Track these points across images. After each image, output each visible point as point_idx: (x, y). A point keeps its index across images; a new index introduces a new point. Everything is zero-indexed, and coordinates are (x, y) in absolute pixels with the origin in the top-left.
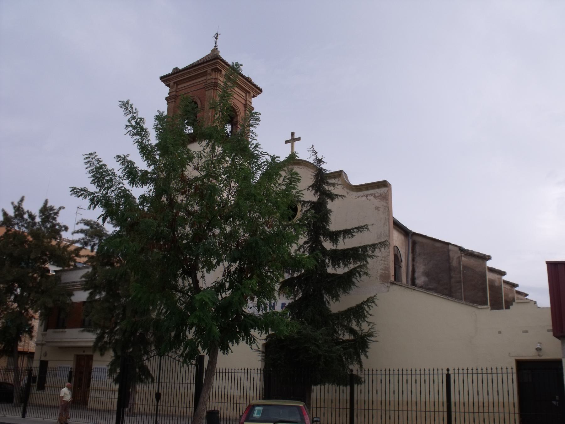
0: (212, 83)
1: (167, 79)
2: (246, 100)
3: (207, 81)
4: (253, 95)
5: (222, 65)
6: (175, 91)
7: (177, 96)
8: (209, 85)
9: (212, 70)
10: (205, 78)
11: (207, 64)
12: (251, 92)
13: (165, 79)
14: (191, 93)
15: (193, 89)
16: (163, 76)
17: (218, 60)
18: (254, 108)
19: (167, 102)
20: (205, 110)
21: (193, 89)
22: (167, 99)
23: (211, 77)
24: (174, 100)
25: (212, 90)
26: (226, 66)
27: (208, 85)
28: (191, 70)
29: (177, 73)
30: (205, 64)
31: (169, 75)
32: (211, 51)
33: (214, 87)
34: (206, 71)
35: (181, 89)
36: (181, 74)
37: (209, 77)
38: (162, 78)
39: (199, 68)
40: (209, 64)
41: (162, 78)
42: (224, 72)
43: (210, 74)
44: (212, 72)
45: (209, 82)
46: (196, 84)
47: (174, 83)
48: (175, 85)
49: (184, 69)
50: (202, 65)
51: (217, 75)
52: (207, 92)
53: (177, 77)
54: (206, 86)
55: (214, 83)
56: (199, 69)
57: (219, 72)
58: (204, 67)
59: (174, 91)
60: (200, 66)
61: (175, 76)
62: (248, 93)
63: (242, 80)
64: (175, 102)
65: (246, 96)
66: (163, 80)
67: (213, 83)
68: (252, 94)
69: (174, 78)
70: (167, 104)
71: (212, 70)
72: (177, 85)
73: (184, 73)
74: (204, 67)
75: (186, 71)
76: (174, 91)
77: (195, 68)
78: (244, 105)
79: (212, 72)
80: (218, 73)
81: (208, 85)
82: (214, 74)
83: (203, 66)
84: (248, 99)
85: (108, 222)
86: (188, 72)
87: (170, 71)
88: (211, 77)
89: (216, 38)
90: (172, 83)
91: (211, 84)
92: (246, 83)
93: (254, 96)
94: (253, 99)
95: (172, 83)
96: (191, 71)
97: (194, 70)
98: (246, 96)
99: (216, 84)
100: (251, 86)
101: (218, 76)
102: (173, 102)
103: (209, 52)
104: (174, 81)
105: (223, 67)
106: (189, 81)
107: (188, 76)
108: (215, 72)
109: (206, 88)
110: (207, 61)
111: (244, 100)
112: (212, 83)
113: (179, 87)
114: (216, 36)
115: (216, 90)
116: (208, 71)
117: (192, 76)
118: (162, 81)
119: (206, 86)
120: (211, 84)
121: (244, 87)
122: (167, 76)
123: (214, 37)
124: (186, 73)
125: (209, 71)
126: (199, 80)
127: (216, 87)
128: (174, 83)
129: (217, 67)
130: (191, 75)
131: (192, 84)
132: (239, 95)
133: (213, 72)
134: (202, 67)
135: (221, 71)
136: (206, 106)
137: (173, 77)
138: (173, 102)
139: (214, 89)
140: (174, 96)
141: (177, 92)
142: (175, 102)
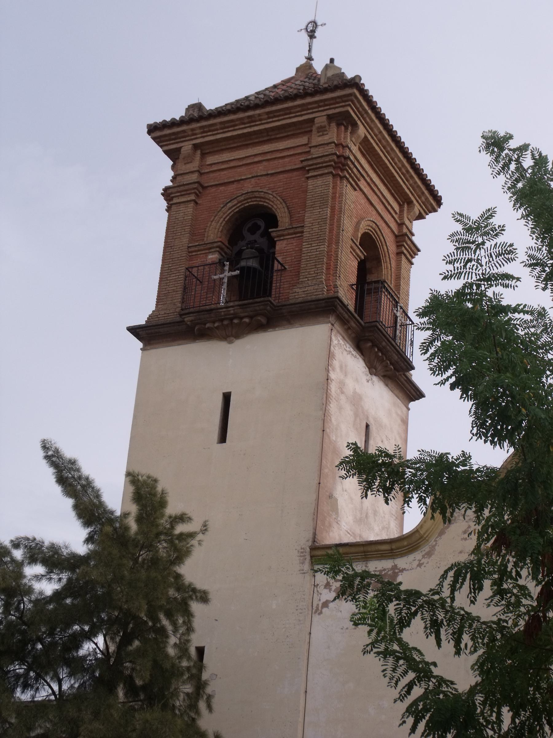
0: (331, 158)
1: (174, 134)
2: (401, 225)
3: (313, 150)
4: (417, 213)
5: (361, 105)
6: (198, 171)
7: (204, 188)
8: (319, 160)
9: (330, 118)
10: (303, 140)
11: (316, 98)
12: (415, 202)
13: (167, 132)
14: (253, 180)
15: (260, 169)
16: (168, 119)
17: (355, 91)
18: (419, 250)
19: (165, 204)
20: (306, 234)
21: (260, 169)
22: (167, 193)
23: (326, 139)
24: (193, 197)
25: (330, 178)
26: (370, 112)
27: (315, 161)
28: (258, 112)
29: (201, 118)
30: (309, 100)
31: (173, 123)
32: (298, 70)
33: (334, 168)
34: (312, 120)
35: (215, 168)
36: (221, 123)
37: (316, 140)
38: (153, 129)
39: (287, 108)
40: (321, 101)
41: (153, 129)
42: (362, 131)
43: (322, 130)
44: (329, 123)
45: (316, 152)
46: (268, 157)
47: (196, 147)
48: (199, 152)
49: (220, 112)
50: (299, 102)
51: (343, 136)
52: (310, 182)
53: (205, 130)
54: (310, 162)
55: (338, 157)
56: (288, 111)
57: (350, 128)
58: (304, 107)
59: (192, 172)
60: (290, 104)
61: (201, 127)
62: (406, 206)
63: (400, 160)
64: (196, 203)
65: (401, 211)
66: (158, 134)
67: (335, 157)
68: (417, 209)
69: (198, 131)
70: (168, 210)
71: (330, 118)
72: (203, 155)
73: (232, 121)
74: (304, 107)
75: (241, 115)
76: (192, 172)
77: (274, 108)
78: (396, 236)
79: (329, 123)
80: (346, 128)
81: (315, 161)
82: (336, 130)
83: (303, 105)
84: (407, 222)
85: (472, 602)
86: (249, 117)
87: (178, 113)
88: (326, 139)
89: (312, 35)
90: (187, 147)
91: (327, 159)
92: (408, 171)
93: (420, 217)
94: (416, 223)
95: (187, 147)
96: (259, 115)
97: (268, 113)
98: (401, 211)
99: (343, 159)
100: (419, 183)
101: (345, 138)
102: (192, 204)
103: (292, 73)
104: (331, 112)
105: (363, 114)
106: (247, 146)
107: (245, 131)
108: (339, 125)
109: (308, 171)
110: (277, 100)
111: (395, 223)
112: (331, 158)
113: (210, 160)
114: (310, 28)
115: (342, 178)
116: (316, 120)
117: (293, 123)
118: (154, 139)
119: (310, 162)
120: (327, 159)
121: (402, 183)
122: (164, 125)
123: (304, 32)
124: (241, 121)
125: (321, 119)
126: (281, 145)
127: (342, 170)
128: (196, 147)
129: (348, 112)
130: (256, 128)
131: (255, 155)
132: (387, 205)
133: (333, 125)
134: (299, 106)
135: (354, 125)
136: (307, 224)
137: (193, 130)
138: (192, 204)
139: (334, 176)
140: (196, 185)
141: (201, 174)
142: (196, 203)
